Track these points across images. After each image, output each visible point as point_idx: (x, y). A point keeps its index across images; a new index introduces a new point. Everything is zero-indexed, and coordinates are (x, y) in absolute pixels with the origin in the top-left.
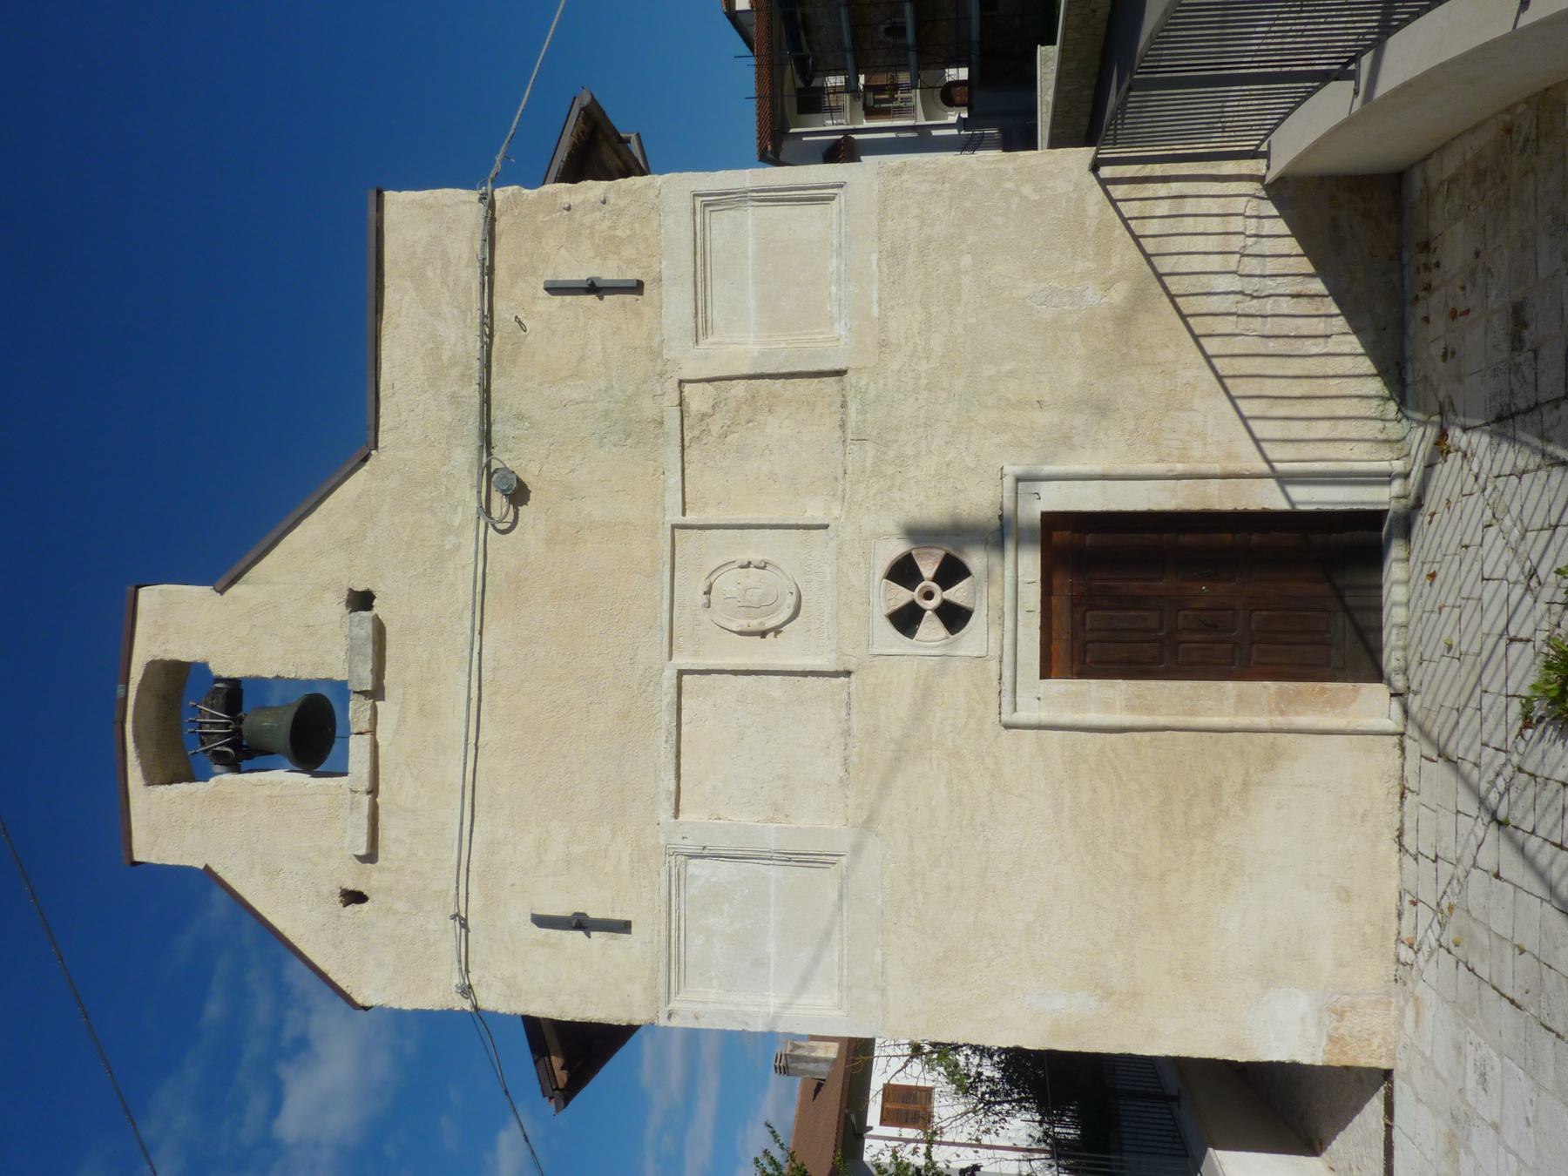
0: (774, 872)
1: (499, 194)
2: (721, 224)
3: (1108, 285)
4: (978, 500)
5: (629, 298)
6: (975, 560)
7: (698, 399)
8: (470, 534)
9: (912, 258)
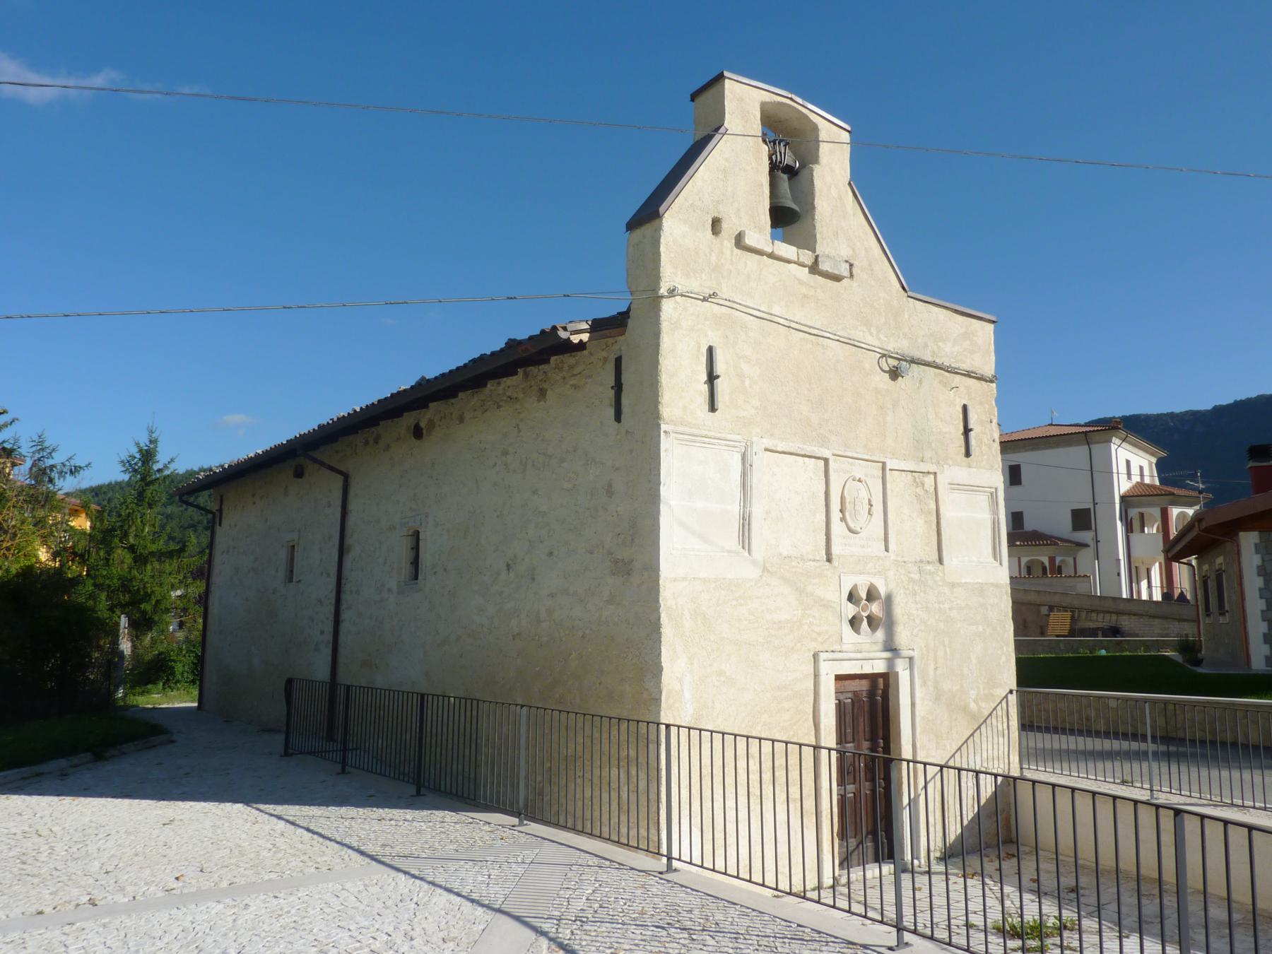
0: (735, 508)
1: (994, 385)
2: (983, 500)
3: (976, 701)
4: (903, 637)
5: (963, 450)
6: (880, 634)
7: (929, 480)
8: (876, 343)
9: (981, 600)
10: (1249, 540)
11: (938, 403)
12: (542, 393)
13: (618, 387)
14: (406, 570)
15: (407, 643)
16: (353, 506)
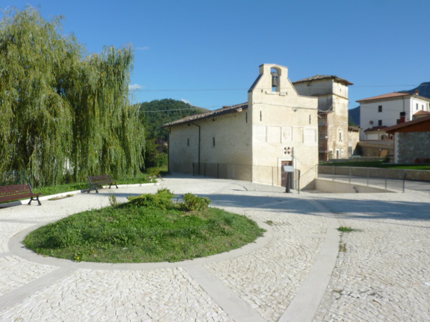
0: (265, 136)
2: (313, 131)
4: (295, 154)
10: (397, 134)
11: (304, 115)
12: (235, 116)
13: (247, 117)
14: (212, 144)
15: (212, 156)
16: (201, 132)
